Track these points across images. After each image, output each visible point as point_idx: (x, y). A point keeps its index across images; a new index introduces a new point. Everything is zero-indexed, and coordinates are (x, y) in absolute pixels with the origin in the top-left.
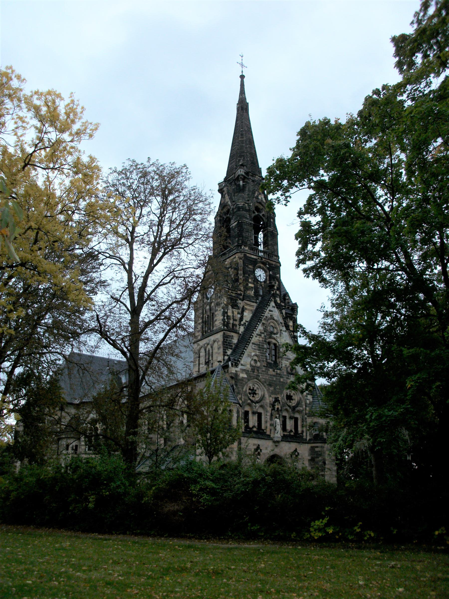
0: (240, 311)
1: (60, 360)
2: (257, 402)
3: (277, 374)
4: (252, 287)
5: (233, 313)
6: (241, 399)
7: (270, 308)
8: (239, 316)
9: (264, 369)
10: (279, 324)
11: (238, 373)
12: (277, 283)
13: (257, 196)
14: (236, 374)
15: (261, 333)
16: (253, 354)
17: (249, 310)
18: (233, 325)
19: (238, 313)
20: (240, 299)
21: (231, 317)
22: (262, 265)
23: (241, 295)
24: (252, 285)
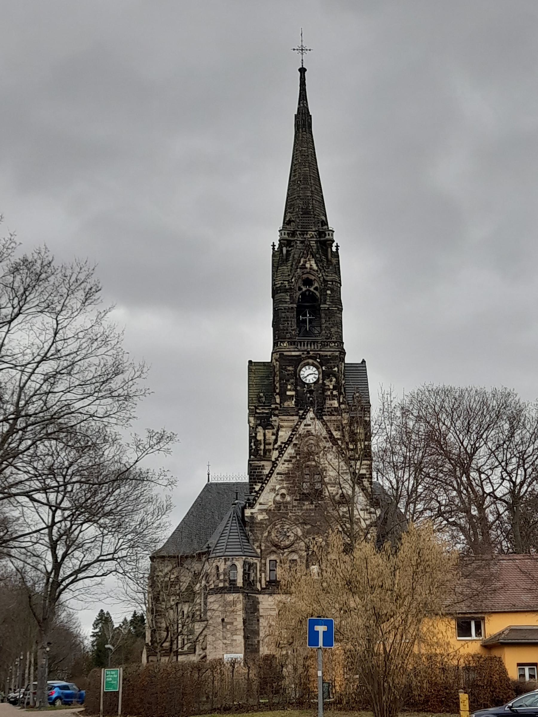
0: (275, 431)
4: (292, 396)
5: (265, 435)
7: (308, 421)
8: (274, 437)
11: (255, 515)
12: (334, 379)
13: (304, 265)
14: (252, 517)
15: (290, 457)
16: (278, 487)
17: (286, 427)
18: (265, 451)
19: (273, 434)
20: (275, 415)
21: (262, 442)
22: (311, 361)
23: (276, 409)
24: (293, 393)
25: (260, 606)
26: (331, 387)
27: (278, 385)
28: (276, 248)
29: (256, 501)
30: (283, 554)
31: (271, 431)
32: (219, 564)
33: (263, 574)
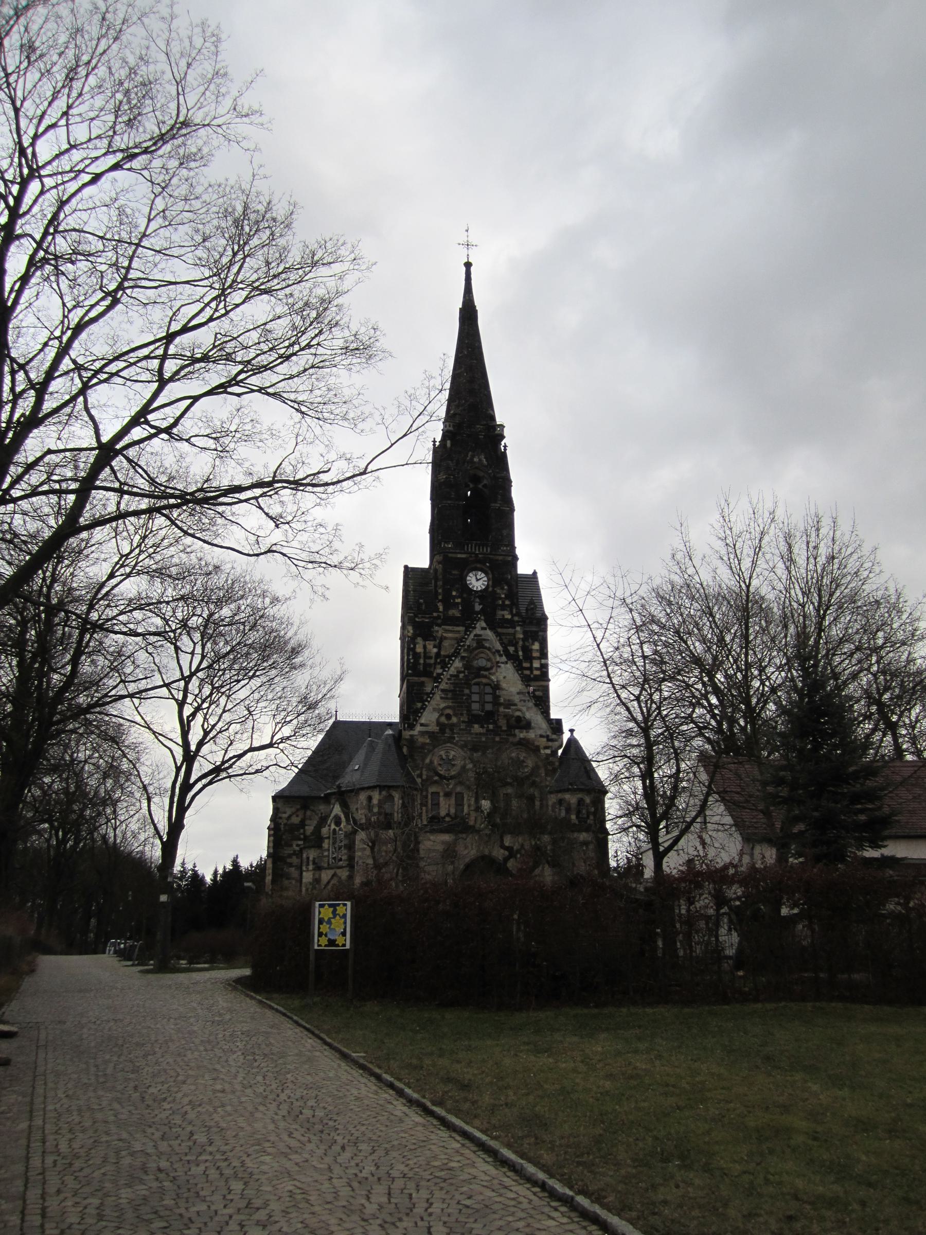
1: (370, 798)
2: (452, 778)
3: (488, 730)
6: (420, 776)
8: (435, 650)
9: (463, 726)
10: (494, 653)
18: (425, 664)
19: (435, 647)
21: (422, 655)
22: (479, 566)
23: (439, 617)
25: (422, 847)
26: (503, 596)
27: (440, 591)
28: (437, 444)
29: (417, 721)
30: (448, 785)
31: (432, 643)
32: (372, 794)
33: (424, 808)
